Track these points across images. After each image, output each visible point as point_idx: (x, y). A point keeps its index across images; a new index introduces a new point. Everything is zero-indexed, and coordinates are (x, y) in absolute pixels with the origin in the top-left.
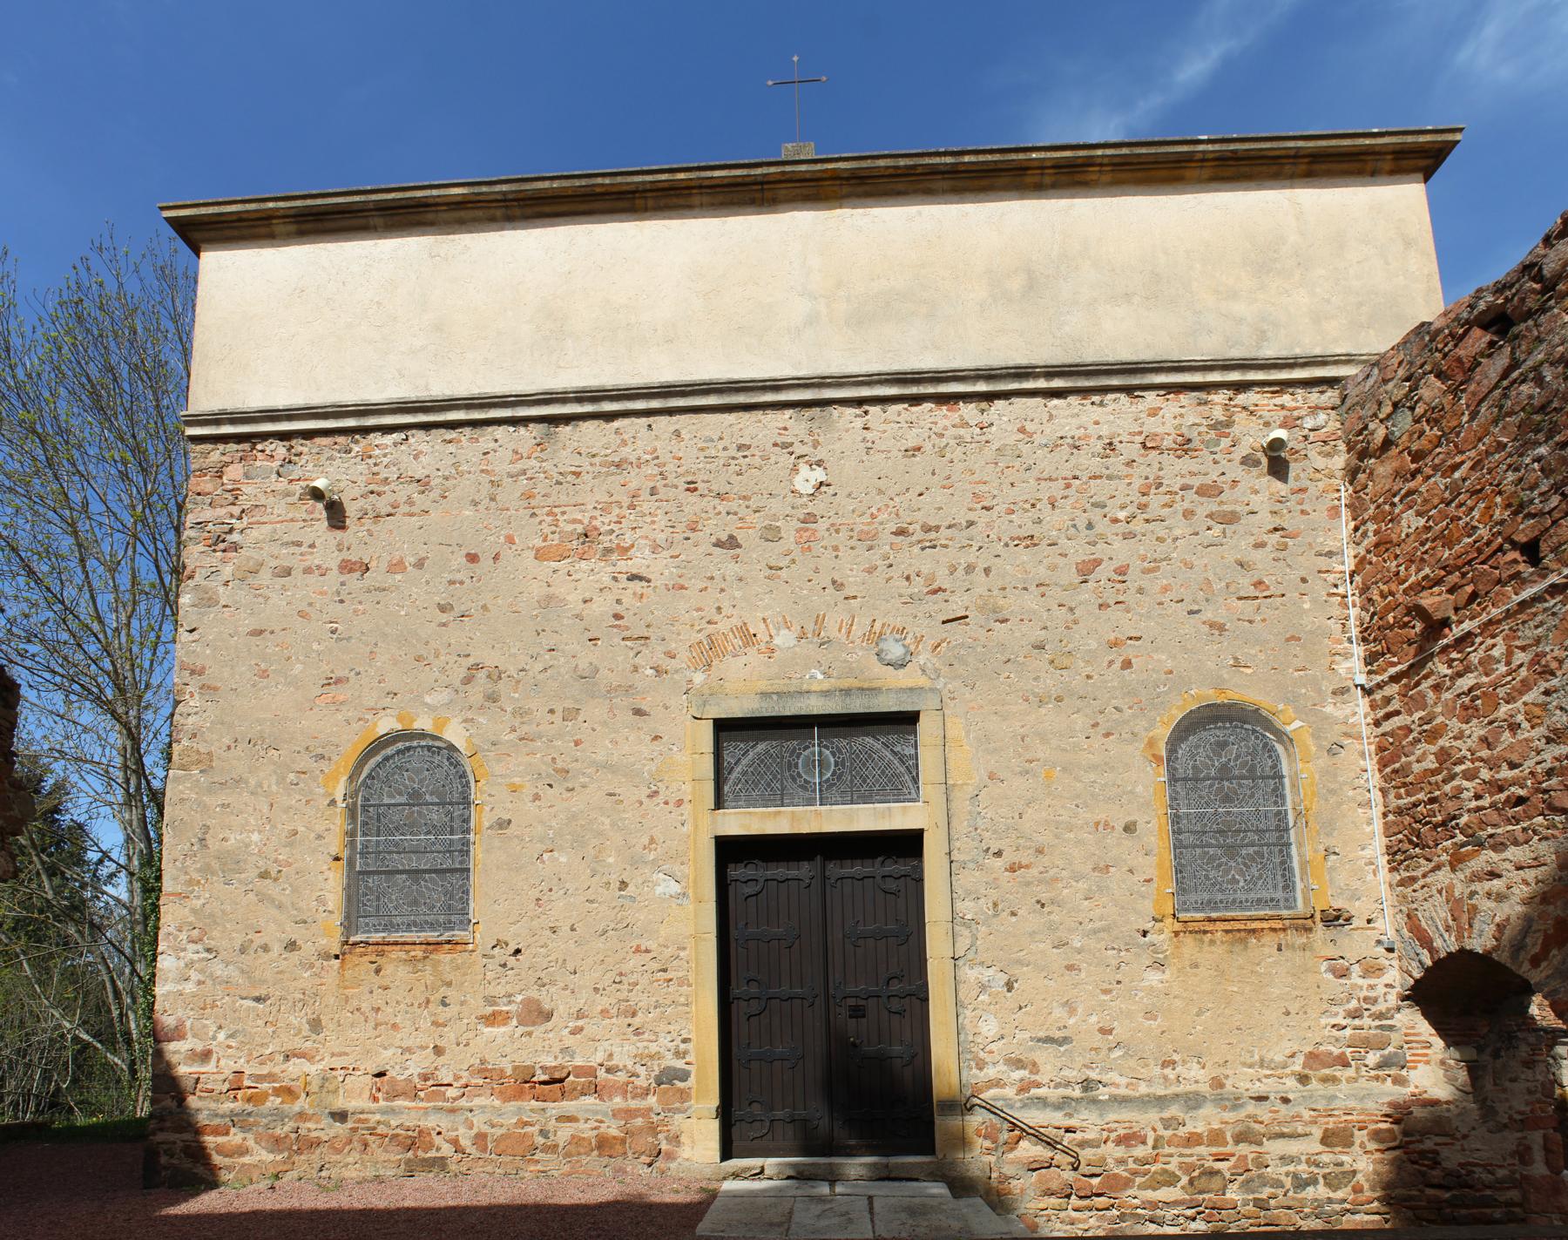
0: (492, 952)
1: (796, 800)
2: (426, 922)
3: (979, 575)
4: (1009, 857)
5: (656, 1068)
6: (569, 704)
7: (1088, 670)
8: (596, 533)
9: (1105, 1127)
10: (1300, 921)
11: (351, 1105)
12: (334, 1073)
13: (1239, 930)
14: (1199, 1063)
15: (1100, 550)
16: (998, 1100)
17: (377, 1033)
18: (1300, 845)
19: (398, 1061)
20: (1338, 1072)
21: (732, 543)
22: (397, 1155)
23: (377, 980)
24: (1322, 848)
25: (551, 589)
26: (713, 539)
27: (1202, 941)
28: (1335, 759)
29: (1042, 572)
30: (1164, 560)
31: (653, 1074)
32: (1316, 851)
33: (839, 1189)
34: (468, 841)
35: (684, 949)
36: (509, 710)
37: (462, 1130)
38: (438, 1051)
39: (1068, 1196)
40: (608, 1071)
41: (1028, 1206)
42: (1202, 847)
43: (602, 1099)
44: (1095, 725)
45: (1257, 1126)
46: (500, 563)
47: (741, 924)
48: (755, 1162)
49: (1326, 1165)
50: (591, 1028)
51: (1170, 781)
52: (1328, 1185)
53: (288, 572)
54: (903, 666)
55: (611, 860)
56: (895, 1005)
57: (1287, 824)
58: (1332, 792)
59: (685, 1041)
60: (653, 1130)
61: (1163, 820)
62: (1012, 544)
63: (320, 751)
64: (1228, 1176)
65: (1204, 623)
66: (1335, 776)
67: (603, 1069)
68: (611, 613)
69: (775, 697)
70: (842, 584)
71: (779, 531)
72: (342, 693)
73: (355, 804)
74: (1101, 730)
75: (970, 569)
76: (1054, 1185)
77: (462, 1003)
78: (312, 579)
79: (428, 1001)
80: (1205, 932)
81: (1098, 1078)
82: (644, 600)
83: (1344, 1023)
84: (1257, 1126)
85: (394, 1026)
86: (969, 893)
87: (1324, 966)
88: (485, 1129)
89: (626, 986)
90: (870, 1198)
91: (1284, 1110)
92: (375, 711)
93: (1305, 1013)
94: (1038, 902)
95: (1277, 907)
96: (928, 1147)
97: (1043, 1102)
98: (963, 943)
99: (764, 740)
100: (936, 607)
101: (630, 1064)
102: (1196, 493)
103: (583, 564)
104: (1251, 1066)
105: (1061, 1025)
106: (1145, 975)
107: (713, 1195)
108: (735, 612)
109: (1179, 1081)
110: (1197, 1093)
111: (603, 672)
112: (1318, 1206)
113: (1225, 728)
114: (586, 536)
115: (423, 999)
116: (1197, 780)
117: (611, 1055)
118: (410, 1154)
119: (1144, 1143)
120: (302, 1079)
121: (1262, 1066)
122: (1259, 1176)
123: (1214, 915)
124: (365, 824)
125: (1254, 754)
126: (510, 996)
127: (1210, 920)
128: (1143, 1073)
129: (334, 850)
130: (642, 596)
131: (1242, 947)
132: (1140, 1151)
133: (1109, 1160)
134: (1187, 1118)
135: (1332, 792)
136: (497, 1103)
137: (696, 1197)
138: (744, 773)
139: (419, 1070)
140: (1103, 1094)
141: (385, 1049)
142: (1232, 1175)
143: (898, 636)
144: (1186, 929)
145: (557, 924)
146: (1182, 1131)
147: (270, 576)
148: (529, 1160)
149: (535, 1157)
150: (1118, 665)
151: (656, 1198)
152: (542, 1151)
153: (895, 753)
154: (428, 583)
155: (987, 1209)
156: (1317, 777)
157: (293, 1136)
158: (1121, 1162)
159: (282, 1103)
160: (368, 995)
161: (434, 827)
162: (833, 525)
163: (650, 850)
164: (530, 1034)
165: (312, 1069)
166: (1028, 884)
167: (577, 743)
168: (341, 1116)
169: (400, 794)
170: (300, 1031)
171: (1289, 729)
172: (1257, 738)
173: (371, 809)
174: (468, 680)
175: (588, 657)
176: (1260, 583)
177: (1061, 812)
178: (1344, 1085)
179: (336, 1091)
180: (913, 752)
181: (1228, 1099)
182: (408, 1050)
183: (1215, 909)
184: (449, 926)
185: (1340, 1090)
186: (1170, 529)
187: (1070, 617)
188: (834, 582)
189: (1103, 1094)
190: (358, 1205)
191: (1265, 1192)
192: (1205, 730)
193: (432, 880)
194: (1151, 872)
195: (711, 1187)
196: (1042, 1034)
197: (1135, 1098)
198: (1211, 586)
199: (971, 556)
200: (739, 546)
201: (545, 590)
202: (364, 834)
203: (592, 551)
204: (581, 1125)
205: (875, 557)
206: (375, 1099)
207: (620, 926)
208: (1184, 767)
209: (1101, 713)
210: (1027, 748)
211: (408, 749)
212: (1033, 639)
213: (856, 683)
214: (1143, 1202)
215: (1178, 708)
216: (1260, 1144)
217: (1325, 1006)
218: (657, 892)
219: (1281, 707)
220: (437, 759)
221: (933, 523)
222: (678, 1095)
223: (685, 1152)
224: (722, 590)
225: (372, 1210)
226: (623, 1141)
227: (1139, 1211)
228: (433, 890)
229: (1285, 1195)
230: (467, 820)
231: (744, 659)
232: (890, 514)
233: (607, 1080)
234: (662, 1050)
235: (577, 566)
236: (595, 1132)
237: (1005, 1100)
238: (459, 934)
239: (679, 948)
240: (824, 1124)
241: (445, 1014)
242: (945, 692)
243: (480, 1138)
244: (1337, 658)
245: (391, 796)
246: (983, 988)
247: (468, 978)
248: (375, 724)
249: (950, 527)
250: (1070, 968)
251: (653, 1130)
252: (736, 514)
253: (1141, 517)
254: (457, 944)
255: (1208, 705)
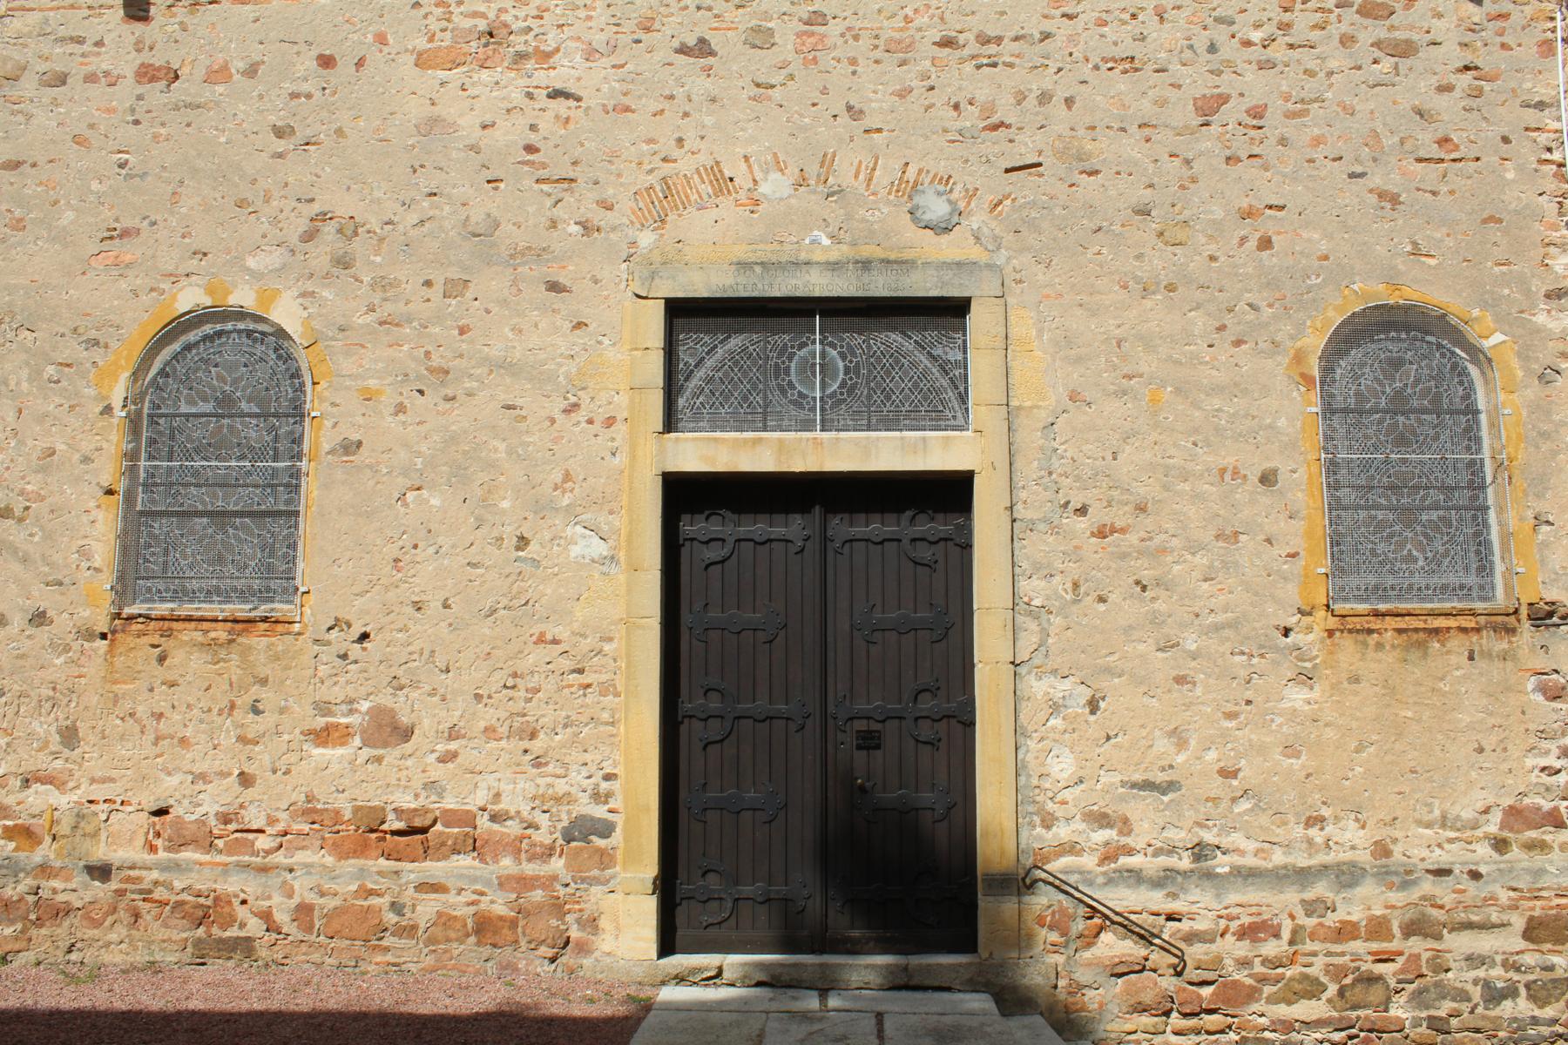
0: (327, 637)
1: (786, 423)
2: (235, 589)
3: (1057, 108)
4: (1097, 516)
5: (564, 816)
6: (454, 273)
7: (1212, 249)
8: (505, 31)
9: (1224, 912)
10: (1500, 619)
11: (118, 855)
12: (93, 807)
13: (1416, 630)
14: (1357, 820)
15: (1227, 84)
16: (1072, 872)
17: (158, 750)
18: (1501, 510)
19: (187, 792)
20: (1549, 835)
21: (703, 48)
22: (181, 932)
23: (160, 673)
24: (1530, 514)
25: (436, 109)
26: (676, 43)
27: (1365, 644)
28: (1549, 390)
29: (1146, 108)
30: (1316, 100)
31: (560, 826)
32: (1522, 519)
33: (834, 1002)
34: (299, 470)
35: (610, 639)
36: (366, 279)
37: (277, 899)
38: (246, 780)
39: (1167, 1014)
40: (494, 818)
41: (1109, 1027)
42: (1367, 508)
43: (483, 861)
44: (1222, 328)
45: (1435, 912)
46: (364, 71)
47: (698, 606)
48: (708, 961)
49: (1530, 969)
50: (468, 756)
51: (1324, 413)
52: (1532, 998)
53: (61, 80)
54: (947, 230)
55: (505, 504)
56: (926, 730)
57: (1483, 478)
58: (1545, 435)
59: (608, 777)
60: (558, 908)
61: (1315, 468)
62: (1104, 67)
63: (93, 334)
64: (1392, 983)
65: (1371, 191)
66: (1548, 413)
67: (486, 816)
68: (522, 143)
69: (758, 269)
70: (861, 112)
71: (772, 36)
72: (129, 251)
73: (139, 413)
74: (1229, 336)
75: (1045, 98)
76: (1148, 998)
77: (282, 711)
78: (95, 90)
79: (233, 706)
80: (1370, 631)
81: (1216, 841)
82: (571, 126)
83: (1558, 764)
84: (1435, 912)
85: (183, 741)
86: (1037, 567)
87: (1531, 683)
88: (311, 898)
89: (522, 694)
90: (880, 1016)
91: (1472, 889)
92: (174, 278)
93: (1505, 750)
94: (1138, 583)
95: (1468, 597)
96: (968, 943)
97: (1136, 877)
98: (1028, 642)
99: (739, 331)
100: (997, 149)
101: (525, 809)
102: (1358, 12)
103: (485, 75)
104: (1428, 825)
105: (1165, 763)
106: (1286, 691)
107: (647, 1007)
108: (703, 145)
109: (1328, 846)
110: (1353, 864)
111: (507, 228)
112: (1519, 1029)
113: (1400, 340)
114: (491, 35)
115: (225, 703)
116: (1361, 412)
117: (498, 795)
118: (201, 931)
119: (1277, 936)
120: (47, 816)
121: (1443, 826)
122: (1437, 985)
123: (1382, 607)
124: (152, 442)
125: (1438, 378)
126: (351, 702)
127: (1377, 614)
128: (1280, 834)
129: (106, 480)
130: (567, 120)
131: (1419, 654)
132: (1271, 948)
133: (1228, 961)
134: (1338, 900)
135: (1545, 435)
136: (329, 860)
137: (622, 1010)
138: (709, 380)
139: (217, 808)
140: (1222, 864)
141: (169, 774)
142: (1399, 982)
143: (941, 188)
144: (1344, 627)
145: (424, 597)
146: (1331, 919)
147: (35, 84)
148: (375, 948)
149: (384, 943)
150: (1252, 244)
151: (557, 1008)
152: (393, 934)
153: (934, 358)
154: (261, 97)
155: (1050, 1032)
156: (1524, 413)
157: (31, 899)
158: (1244, 963)
159: (16, 849)
160: (147, 694)
161: (252, 449)
162: (849, 29)
163: (564, 492)
164: (379, 760)
165: (63, 800)
166: (1124, 556)
167: (462, 331)
168: (101, 872)
169: (205, 400)
170: (46, 744)
171: (1487, 344)
172: (1443, 355)
173: (162, 421)
174: (309, 237)
175: (482, 206)
176: (1447, 140)
177: (1172, 451)
178: (1556, 855)
179: (95, 835)
180: (960, 357)
181: (1396, 873)
182: (202, 777)
183: (1385, 599)
184: (266, 595)
185: (1551, 862)
186: (1324, 59)
187: (1186, 172)
188: (849, 108)
189: (1222, 864)
190: (120, 1005)
191: (1442, 1011)
192: (1373, 341)
193: (244, 527)
194: (1297, 544)
195: (642, 996)
196: (1138, 777)
197: (1267, 870)
198: (1379, 141)
199: (1047, 81)
200: (712, 53)
201: (429, 110)
202: (151, 457)
203: (497, 58)
204: (452, 898)
205: (910, 76)
206: (153, 849)
207: (516, 603)
208: (1344, 393)
209: (1230, 311)
210: (1124, 358)
211: (219, 334)
212: (1134, 200)
213: (879, 253)
214: (1273, 1022)
215: (1336, 309)
216: (1439, 937)
217: (1532, 740)
218: (573, 554)
219: (1476, 312)
220: (259, 349)
221: (992, 32)
222: (597, 858)
223: (605, 943)
224: (686, 115)
225: (140, 1012)
226: (514, 924)
227: (1267, 1034)
228: (246, 543)
229: (1472, 1012)
230: (298, 441)
231: (713, 213)
232: (932, 17)
233: (490, 832)
234: (573, 790)
235: (475, 79)
236: (472, 909)
237: (1081, 873)
238: (280, 608)
239: (602, 639)
240: (815, 905)
241: (255, 725)
242: (1008, 270)
243: (303, 912)
244: (1552, 249)
245: (191, 402)
246: (1055, 708)
247: (292, 673)
248: (174, 298)
249: (1016, 39)
250: (1180, 680)
251: (558, 908)
252: (710, 9)
253: (1283, 40)
254: (277, 622)
255: (1377, 307)
